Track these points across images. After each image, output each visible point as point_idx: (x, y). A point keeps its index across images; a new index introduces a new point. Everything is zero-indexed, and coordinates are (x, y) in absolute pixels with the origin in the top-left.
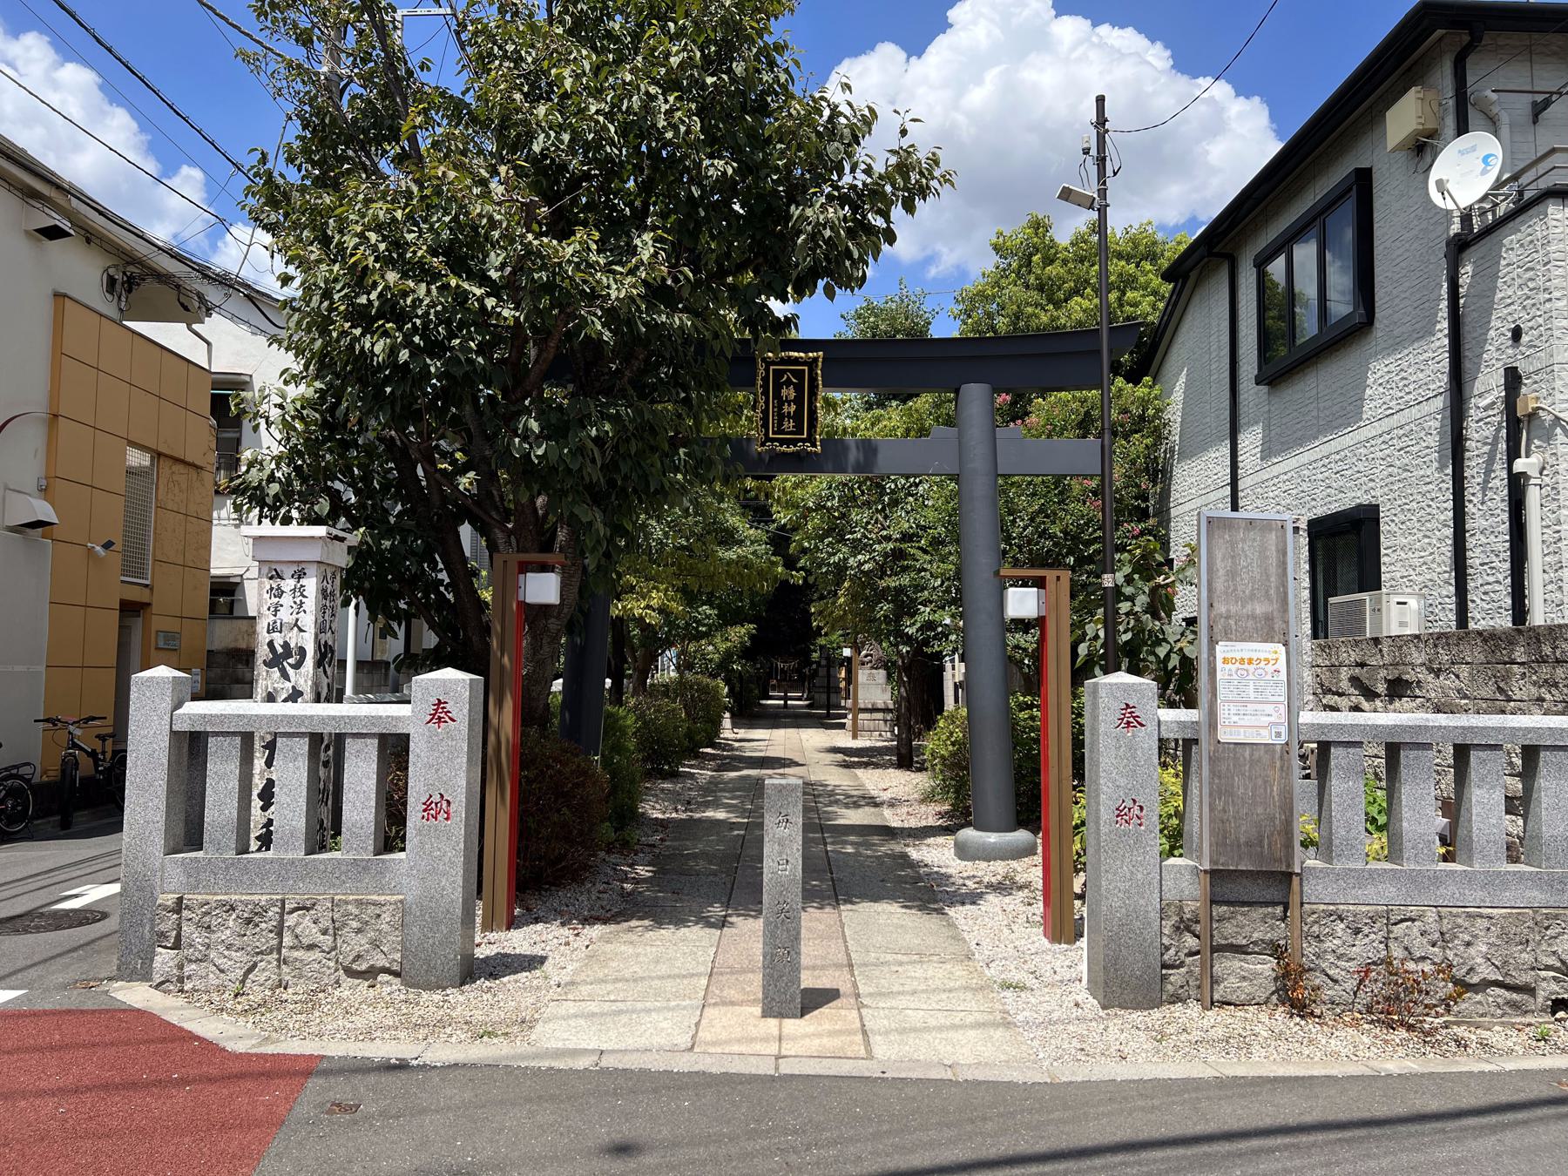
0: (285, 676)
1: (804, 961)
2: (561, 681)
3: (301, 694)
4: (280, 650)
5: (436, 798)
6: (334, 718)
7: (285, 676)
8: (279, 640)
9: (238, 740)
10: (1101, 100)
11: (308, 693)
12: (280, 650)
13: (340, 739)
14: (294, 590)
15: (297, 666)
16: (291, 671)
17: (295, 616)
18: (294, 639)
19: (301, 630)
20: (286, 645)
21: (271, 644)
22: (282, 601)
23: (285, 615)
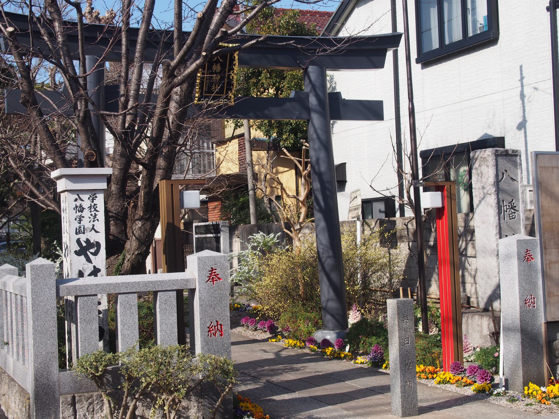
0: (89, 260)
1: (419, 398)
2: (52, 162)
3: (99, 270)
4: (84, 244)
5: (215, 323)
6: (151, 282)
7: (89, 260)
8: (83, 237)
9: (175, 292)
10: (521, 67)
11: (103, 271)
12: (84, 244)
13: (155, 293)
14: (90, 207)
15: (95, 254)
16: (92, 257)
17: (92, 223)
18: (93, 237)
19: (97, 232)
20: (88, 241)
21: (78, 241)
22: (83, 214)
23: (86, 223)
